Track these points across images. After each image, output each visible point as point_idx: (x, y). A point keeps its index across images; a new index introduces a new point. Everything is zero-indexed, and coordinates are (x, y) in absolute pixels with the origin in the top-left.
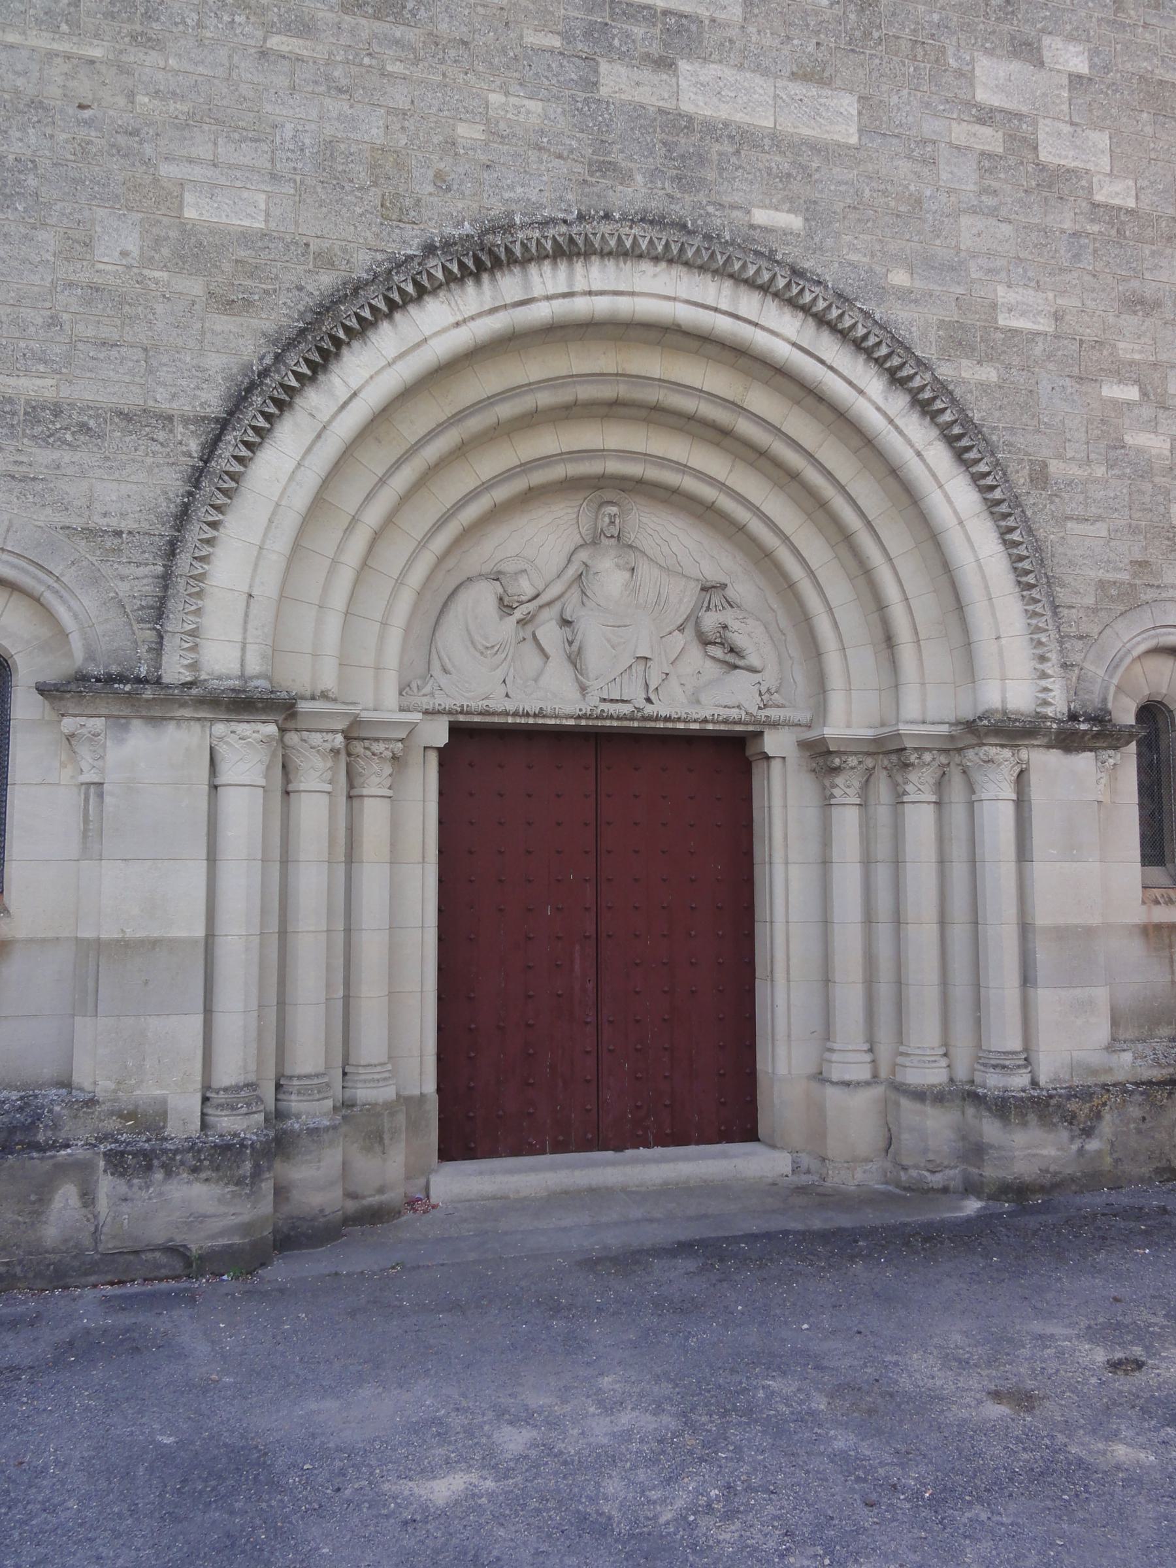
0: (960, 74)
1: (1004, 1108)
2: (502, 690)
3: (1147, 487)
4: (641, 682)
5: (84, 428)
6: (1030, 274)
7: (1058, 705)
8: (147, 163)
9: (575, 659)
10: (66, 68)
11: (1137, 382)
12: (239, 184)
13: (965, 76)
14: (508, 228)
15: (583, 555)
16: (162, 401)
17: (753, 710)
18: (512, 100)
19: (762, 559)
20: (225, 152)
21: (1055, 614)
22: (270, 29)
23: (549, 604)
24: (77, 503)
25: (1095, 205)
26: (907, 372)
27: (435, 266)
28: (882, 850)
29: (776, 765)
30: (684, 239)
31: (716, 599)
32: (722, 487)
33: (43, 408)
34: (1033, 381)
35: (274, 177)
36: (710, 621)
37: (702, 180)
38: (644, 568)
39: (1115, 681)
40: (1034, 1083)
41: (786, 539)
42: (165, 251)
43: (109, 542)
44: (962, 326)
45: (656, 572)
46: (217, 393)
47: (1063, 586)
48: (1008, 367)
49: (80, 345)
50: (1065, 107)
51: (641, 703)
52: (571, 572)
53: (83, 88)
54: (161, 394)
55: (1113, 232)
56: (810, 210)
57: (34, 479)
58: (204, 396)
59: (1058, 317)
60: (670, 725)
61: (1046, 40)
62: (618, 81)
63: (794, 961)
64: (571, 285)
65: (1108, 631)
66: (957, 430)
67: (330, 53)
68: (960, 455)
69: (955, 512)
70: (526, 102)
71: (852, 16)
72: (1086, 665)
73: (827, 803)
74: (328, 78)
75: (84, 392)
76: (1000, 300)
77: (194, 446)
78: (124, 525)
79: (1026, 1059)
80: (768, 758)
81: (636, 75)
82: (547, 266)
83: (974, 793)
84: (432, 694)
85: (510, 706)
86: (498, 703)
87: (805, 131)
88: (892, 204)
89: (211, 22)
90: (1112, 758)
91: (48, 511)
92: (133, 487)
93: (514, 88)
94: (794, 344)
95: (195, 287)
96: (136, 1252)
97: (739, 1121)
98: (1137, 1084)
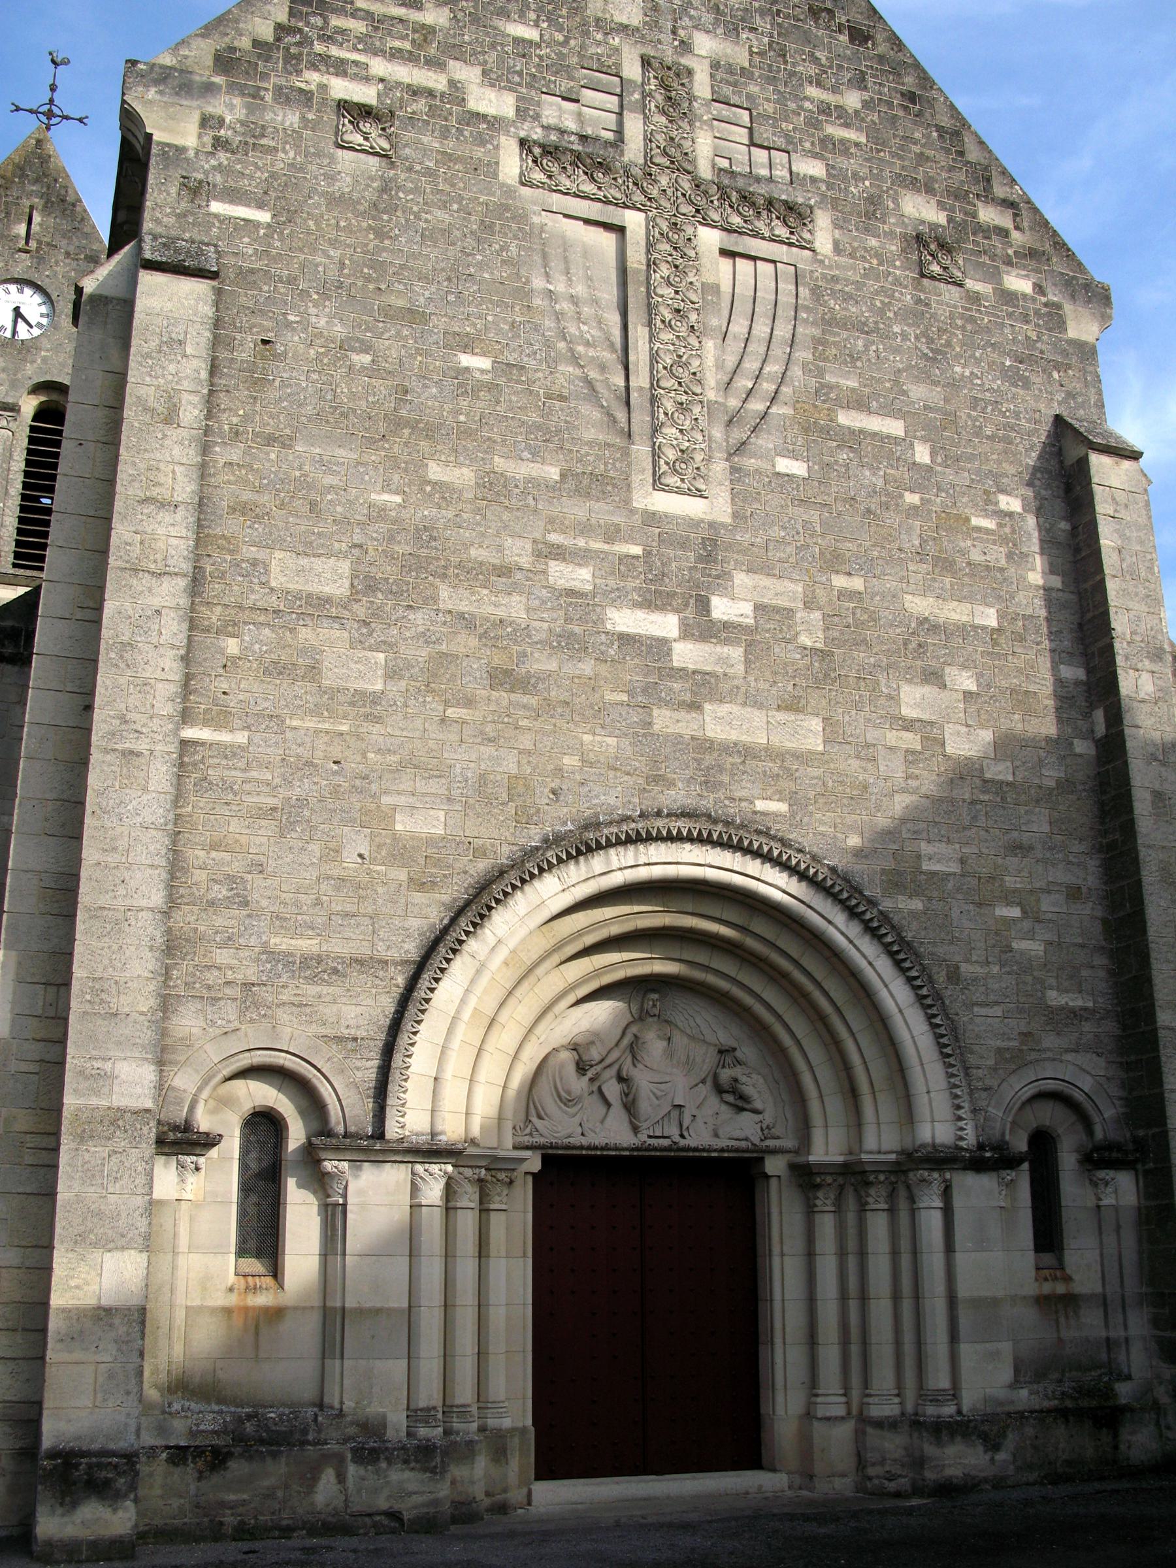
0: (890, 697)
1: (942, 1430)
2: (579, 1130)
3: (1029, 979)
4: (676, 1123)
5: (335, 971)
6: (943, 832)
7: (970, 1138)
8: (373, 796)
9: (630, 1107)
10: (326, 739)
11: (1019, 904)
12: (428, 806)
13: (894, 698)
14: (598, 825)
15: (634, 1029)
16: (382, 951)
17: (757, 1142)
18: (598, 738)
19: (760, 1031)
20: (421, 786)
21: (967, 1074)
22: (447, 704)
23: (609, 1066)
24: (331, 1020)
25: (985, 781)
26: (861, 908)
27: (551, 855)
28: (852, 1245)
29: (774, 1183)
30: (711, 827)
31: (729, 1059)
32: (734, 981)
33: (311, 959)
34: (947, 908)
35: (449, 800)
36: (726, 1075)
37: (721, 783)
38: (678, 1038)
39: (1010, 1119)
40: (959, 1412)
41: (779, 1017)
42: (384, 853)
43: (350, 1045)
44: (899, 873)
45: (685, 1040)
46: (414, 944)
47: (972, 1053)
48: (930, 899)
49: (333, 917)
50: (962, 715)
51: (677, 1138)
52: (626, 1041)
53: (336, 752)
54: (381, 946)
55: (999, 799)
56: (792, 799)
57: (306, 1005)
58: (406, 946)
59: (962, 861)
60: (697, 1154)
61: (947, 670)
62: (665, 720)
63: (788, 1330)
64: (636, 860)
65: (1005, 1084)
66: (895, 948)
67: (484, 717)
68: (898, 964)
69: (897, 1005)
70: (606, 739)
71: (816, 664)
72: (990, 1109)
73: (810, 1211)
74: (482, 733)
75: (338, 947)
76: (923, 853)
77: (401, 980)
78: (360, 1033)
79: (953, 1395)
80: (767, 1177)
81: (676, 715)
82: (621, 849)
83: (914, 1202)
84: (531, 1134)
85: (584, 1141)
86: (577, 1140)
87: (788, 744)
88: (848, 790)
89: (411, 702)
90: (1009, 1175)
91: (314, 1026)
92: (365, 1009)
93: (599, 730)
94: (784, 892)
95: (402, 875)
96: (370, 1515)
97: (748, 1451)
98: (1031, 1412)
